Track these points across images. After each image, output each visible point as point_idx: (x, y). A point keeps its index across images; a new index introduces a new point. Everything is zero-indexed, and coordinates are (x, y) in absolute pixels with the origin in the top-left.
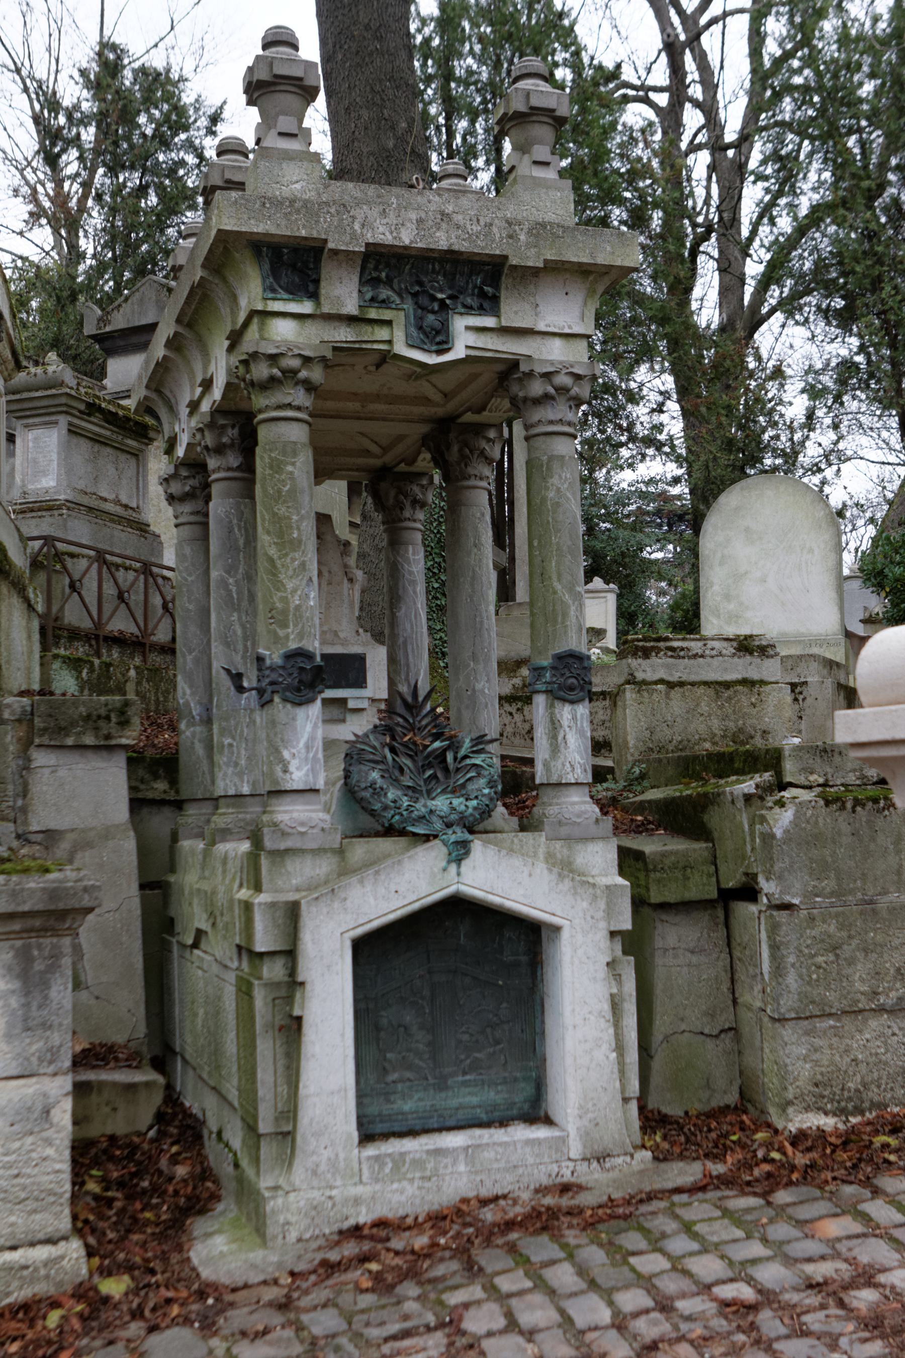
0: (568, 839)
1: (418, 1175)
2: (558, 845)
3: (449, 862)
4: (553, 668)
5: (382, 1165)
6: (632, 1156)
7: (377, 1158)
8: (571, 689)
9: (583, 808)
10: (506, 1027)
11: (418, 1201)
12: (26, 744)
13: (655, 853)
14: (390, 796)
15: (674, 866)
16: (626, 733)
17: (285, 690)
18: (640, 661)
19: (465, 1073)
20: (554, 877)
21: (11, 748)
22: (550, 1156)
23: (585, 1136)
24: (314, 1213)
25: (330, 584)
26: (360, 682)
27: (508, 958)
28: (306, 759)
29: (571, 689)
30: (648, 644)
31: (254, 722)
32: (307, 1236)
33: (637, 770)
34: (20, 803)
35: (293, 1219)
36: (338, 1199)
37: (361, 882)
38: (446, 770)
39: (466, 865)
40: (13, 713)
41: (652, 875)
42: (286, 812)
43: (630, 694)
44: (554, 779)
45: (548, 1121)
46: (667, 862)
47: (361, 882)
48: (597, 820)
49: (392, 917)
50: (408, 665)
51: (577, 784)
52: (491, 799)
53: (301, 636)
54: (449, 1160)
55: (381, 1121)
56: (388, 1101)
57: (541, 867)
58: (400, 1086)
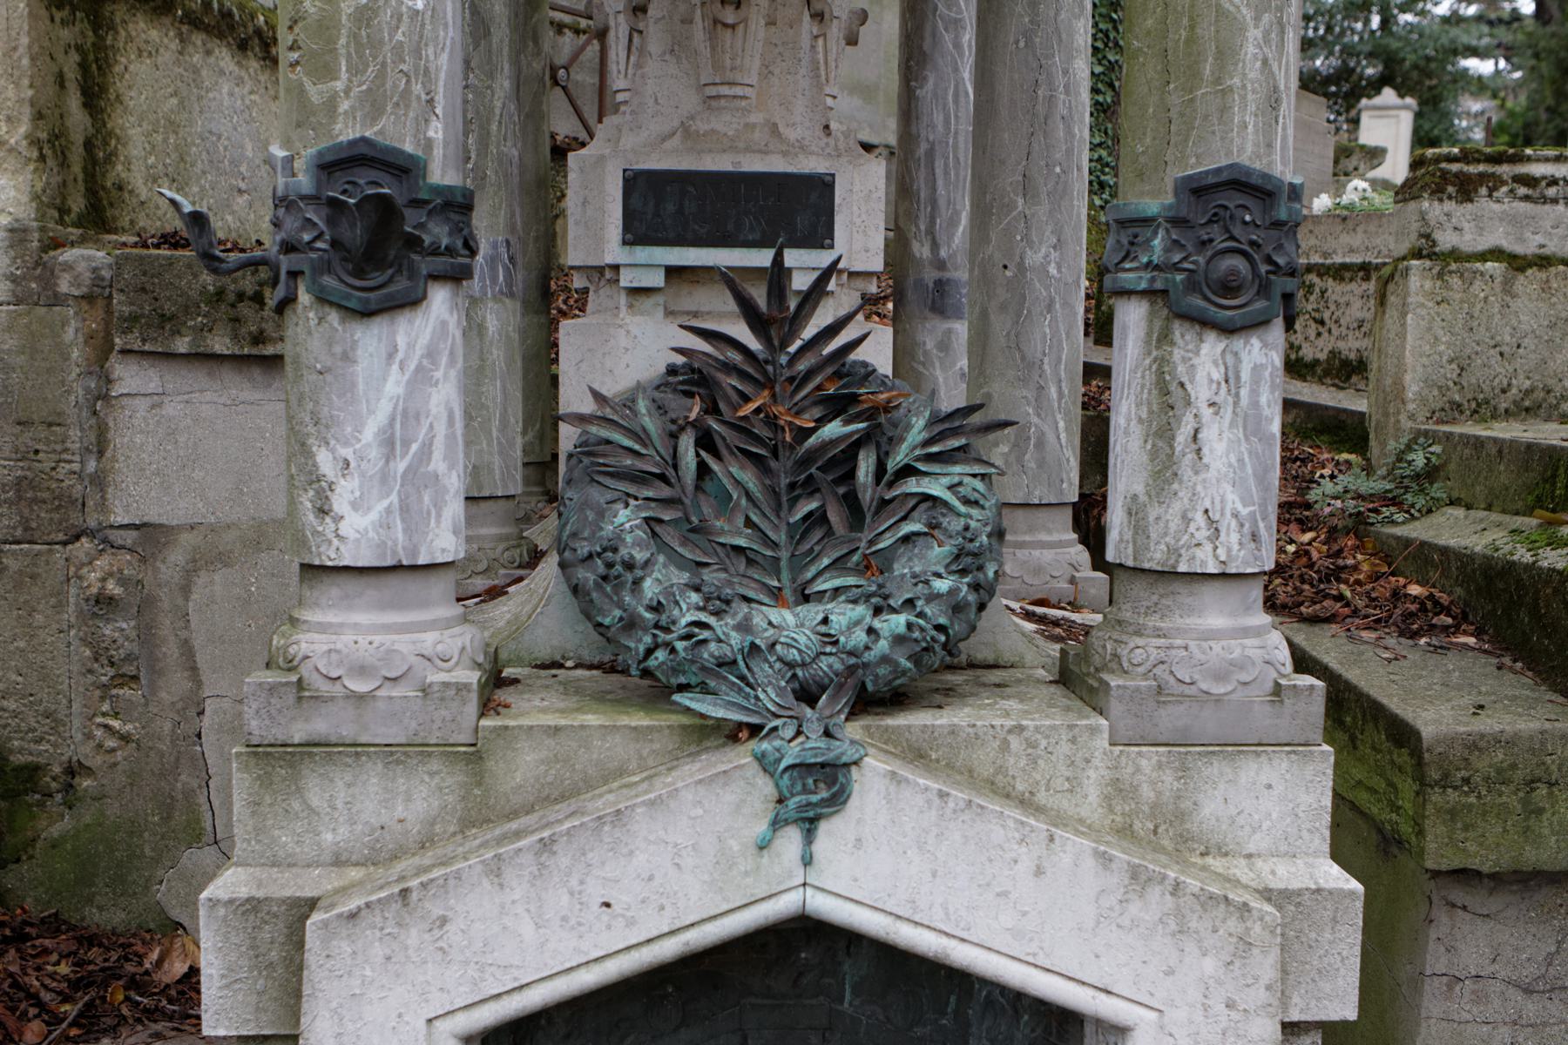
0: (1180, 744)
2: (1147, 759)
3: (777, 824)
4: (1177, 222)
8: (1228, 288)
12: (102, 350)
13: (1451, 740)
14: (650, 588)
15: (1501, 777)
16: (1401, 368)
17: (325, 267)
18: (1449, 206)
20: (1116, 880)
21: (75, 354)
25: (771, 23)
26: (819, 234)
28: (384, 478)
29: (1228, 288)
30: (1473, 169)
31: (481, 329)
33: (1419, 459)
34: (92, 466)
37: (495, 870)
38: (852, 502)
39: (831, 833)
40: (76, 282)
41: (1435, 796)
42: (323, 628)
43: (1418, 279)
44: (1155, 558)
46: (1482, 764)
47: (495, 870)
48: (1278, 690)
49: (589, 979)
50: (934, 202)
52: (957, 609)
53: (374, 104)
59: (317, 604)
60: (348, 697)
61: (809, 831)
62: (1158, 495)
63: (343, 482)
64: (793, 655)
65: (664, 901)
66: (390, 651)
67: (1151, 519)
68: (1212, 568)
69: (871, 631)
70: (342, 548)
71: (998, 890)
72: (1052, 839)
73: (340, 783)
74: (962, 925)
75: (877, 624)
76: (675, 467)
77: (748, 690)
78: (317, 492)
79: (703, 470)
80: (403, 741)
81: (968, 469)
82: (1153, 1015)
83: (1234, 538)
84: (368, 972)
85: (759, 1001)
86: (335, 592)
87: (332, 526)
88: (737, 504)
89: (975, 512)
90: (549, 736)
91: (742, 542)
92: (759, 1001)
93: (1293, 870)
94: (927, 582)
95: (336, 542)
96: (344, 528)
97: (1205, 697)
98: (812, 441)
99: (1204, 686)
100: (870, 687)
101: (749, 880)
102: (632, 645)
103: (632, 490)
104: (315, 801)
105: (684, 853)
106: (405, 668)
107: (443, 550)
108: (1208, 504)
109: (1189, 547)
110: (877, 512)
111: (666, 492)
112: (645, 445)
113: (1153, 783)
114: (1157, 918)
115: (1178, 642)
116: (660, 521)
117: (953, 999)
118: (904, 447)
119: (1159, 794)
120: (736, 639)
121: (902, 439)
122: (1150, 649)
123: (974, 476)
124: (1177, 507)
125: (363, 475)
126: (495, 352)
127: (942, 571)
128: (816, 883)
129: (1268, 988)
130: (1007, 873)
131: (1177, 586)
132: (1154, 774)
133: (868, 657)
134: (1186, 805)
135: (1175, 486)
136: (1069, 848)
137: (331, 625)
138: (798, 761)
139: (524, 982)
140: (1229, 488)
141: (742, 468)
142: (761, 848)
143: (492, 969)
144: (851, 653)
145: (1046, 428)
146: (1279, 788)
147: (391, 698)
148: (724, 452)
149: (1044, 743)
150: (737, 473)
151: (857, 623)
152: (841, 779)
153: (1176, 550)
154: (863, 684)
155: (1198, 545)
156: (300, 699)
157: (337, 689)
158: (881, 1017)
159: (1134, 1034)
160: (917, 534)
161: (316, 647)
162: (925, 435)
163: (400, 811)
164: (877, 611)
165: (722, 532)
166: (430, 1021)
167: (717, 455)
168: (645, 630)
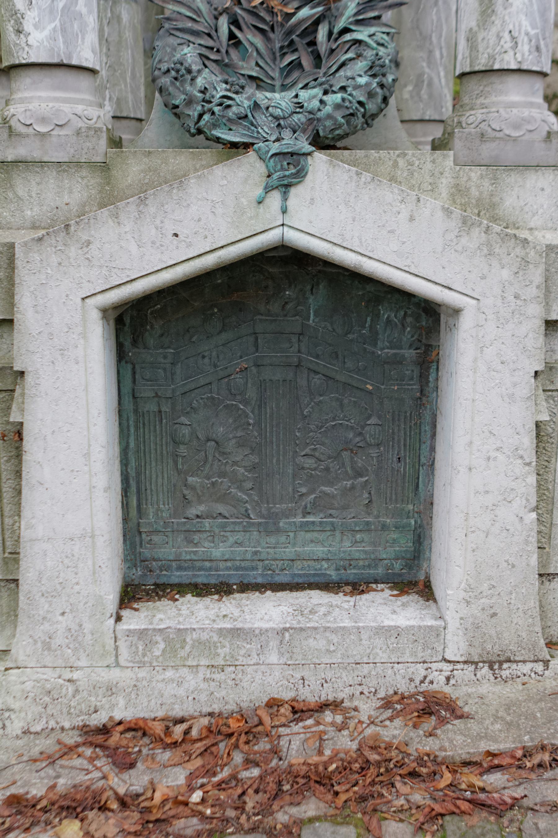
0: (495, 166)
1: (204, 662)
2: (475, 173)
3: (268, 189)
5: (150, 644)
6: (546, 663)
7: (142, 633)
9: (526, 113)
10: (374, 452)
11: (203, 697)
14: (200, 82)
19: (306, 513)
20: (454, 224)
22: (414, 654)
23: (473, 629)
24: (47, 699)
27: (383, 351)
31: (119, 19)
32: (38, 728)
35: (16, 705)
36: (82, 684)
44: (481, 64)
45: (427, 591)
51: (519, 71)
54: (254, 646)
55: (180, 568)
56: (190, 541)
57: (432, 208)
58: (207, 523)
59: (19, 90)
60: (36, 135)
61: (285, 192)
62: (484, 25)
63: (29, 13)
64: (278, 112)
65: (207, 233)
66: (58, 110)
67: (480, 40)
68: (513, 66)
69: (321, 102)
70: (30, 52)
71: (389, 229)
72: (419, 200)
73: (34, 183)
74: (369, 248)
75: (325, 98)
76: (216, 31)
77: (253, 128)
78: (16, 21)
79: (232, 36)
80: (67, 160)
81: (379, 29)
82: (474, 302)
83: (526, 48)
84: (49, 272)
85: (264, 318)
86: (28, 81)
87: (24, 40)
88: (251, 55)
89: (381, 48)
90: (145, 156)
91: (254, 74)
92: (264, 318)
93: (555, 236)
94: (353, 78)
95: (26, 48)
96: (31, 40)
97: (508, 138)
98: (293, 20)
99: (507, 132)
100: (321, 134)
101: (253, 222)
102: (191, 113)
103: (192, 39)
104: (20, 193)
105: (217, 206)
106: (67, 120)
107: (86, 59)
108: (511, 27)
109: (500, 54)
110: (328, 57)
111: (210, 43)
112: (199, 16)
113: (478, 187)
114: (476, 246)
115: (494, 109)
116: (208, 58)
117: (369, 319)
118: (344, 19)
119: (481, 193)
120: (246, 103)
121: (342, 15)
122: (478, 115)
123: (384, 33)
124: (494, 30)
125: (39, 8)
126: (127, 35)
127: (362, 74)
128: (289, 224)
129: (538, 287)
130: (394, 219)
131: (494, 78)
132: (479, 182)
133: (320, 115)
134: (496, 199)
135: (493, 18)
136: (428, 205)
137: (26, 98)
138: (278, 151)
139: (133, 278)
140: (524, 18)
141: (254, 36)
142: (260, 203)
143: (116, 270)
144: (310, 112)
145: (433, 75)
146: (548, 190)
147: (59, 135)
148: (244, 27)
149: (417, 163)
150: (250, 37)
151: (314, 97)
152: (302, 162)
153: (493, 56)
154: (317, 131)
155: (506, 52)
156: (10, 136)
157: (30, 130)
158: (330, 328)
159: (463, 312)
160: (351, 60)
161: (18, 110)
162: (355, 11)
163: (66, 199)
164: (326, 93)
165: (243, 68)
166: (83, 299)
167: (239, 28)
168: (197, 103)
